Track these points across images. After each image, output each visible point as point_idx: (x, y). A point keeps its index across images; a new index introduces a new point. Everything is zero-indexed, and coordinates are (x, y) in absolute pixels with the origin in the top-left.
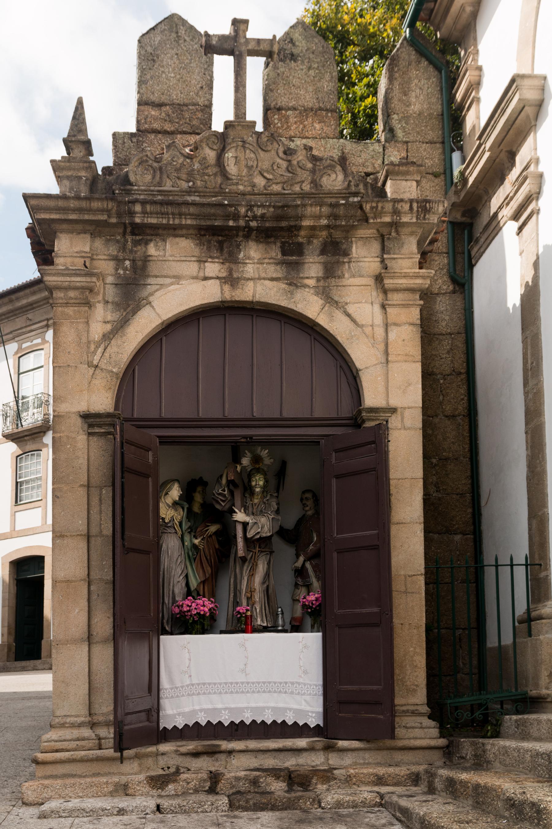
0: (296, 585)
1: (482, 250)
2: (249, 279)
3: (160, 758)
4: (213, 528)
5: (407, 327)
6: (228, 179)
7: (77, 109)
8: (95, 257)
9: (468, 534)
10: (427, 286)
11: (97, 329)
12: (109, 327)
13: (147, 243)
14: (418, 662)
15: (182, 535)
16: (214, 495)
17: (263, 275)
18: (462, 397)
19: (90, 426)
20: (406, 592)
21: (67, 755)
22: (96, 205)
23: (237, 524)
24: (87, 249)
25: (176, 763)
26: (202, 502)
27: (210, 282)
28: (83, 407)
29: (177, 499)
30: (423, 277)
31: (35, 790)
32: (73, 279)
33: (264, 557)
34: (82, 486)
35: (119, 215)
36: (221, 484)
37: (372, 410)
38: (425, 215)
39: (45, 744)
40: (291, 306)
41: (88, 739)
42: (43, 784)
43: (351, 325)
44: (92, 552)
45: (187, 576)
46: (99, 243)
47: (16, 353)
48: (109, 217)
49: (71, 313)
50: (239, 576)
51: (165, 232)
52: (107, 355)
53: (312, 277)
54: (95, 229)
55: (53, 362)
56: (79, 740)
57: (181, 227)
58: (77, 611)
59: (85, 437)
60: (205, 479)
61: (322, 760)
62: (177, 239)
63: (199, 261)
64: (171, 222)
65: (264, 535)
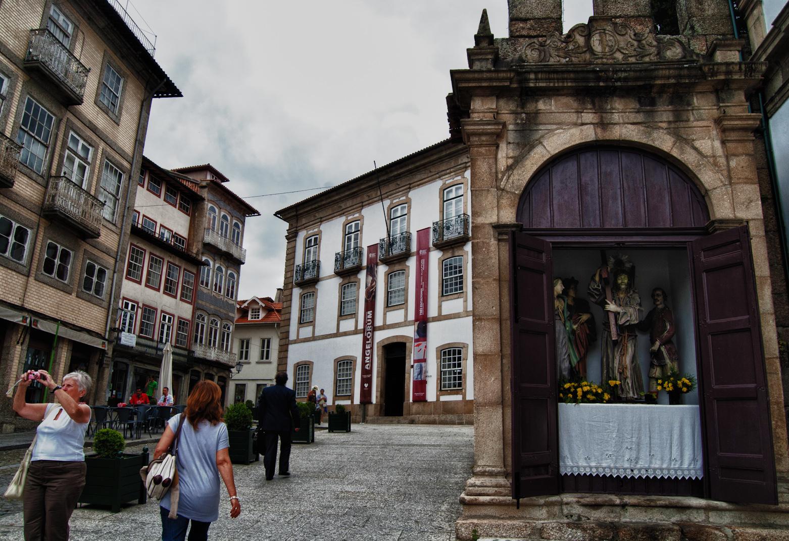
1: (777, 106)
2: (615, 124)
3: (564, 507)
4: (585, 317)
6: (595, 55)
7: (483, 16)
8: (500, 112)
10: (757, 125)
11: (503, 162)
13: (537, 101)
14: (780, 434)
15: (565, 322)
16: (590, 290)
17: (626, 121)
18: (771, 217)
19: (500, 234)
21: (487, 498)
22: (502, 75)
23: (610, 314)
24: (494, 107)
25: (578, 512)
27: (585, 127)
28: (493, 219)
29: (561, 293)
30: (754, 119)
31: (466, 528)
32: (485, 127)
33: (631, 341)
34: (494, 280)
35: (520, 82)
36: (595, 281)
37: (722, 221)
38: (751, 74)
39: (470, 488)
40: (650, 143)
41: (504, 487)
42: (473, 523)
44: (503, 332)
46: (502, 103)
47: (389, 206)
48: (511, 83)
49: (484, 151)
50: (611, 356)
51: (551, 93)
52: (510, 181)
53: (665, 121)
54: (499, 93)
55: (471, 187)
56: (497, 487)
57: (563, 88)
58: (493, 379)
59: (496, 242)
60: (576, 279)
61: (704, 518)
62: (560, 98)
63: (577, 112)
64: (556, 85)
65: (633, 323)
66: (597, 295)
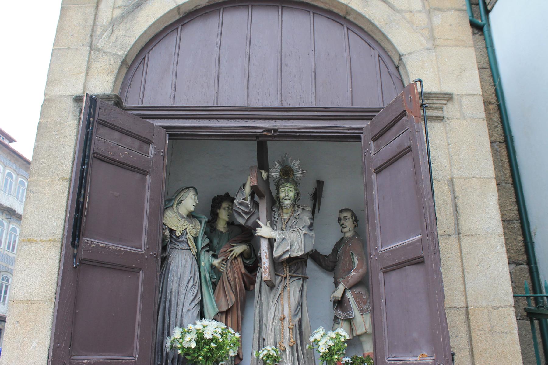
0: (336, 319)
4: (239, 249)
5: (452, 12)
9: (522, 264)
12: (118, 12)
18: (496, 124)
20: (491, 331)
26: (227, 220)
43: (390, 11)
45: (201, 303)
50: (265, 306)
52: (113, 38)
65: (294, 255)
66: (246, 213)
